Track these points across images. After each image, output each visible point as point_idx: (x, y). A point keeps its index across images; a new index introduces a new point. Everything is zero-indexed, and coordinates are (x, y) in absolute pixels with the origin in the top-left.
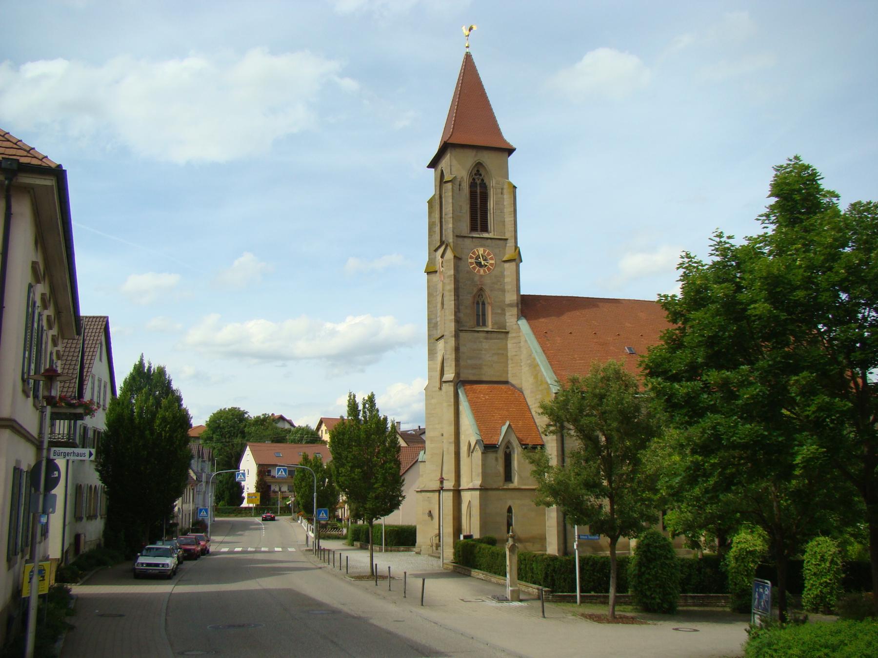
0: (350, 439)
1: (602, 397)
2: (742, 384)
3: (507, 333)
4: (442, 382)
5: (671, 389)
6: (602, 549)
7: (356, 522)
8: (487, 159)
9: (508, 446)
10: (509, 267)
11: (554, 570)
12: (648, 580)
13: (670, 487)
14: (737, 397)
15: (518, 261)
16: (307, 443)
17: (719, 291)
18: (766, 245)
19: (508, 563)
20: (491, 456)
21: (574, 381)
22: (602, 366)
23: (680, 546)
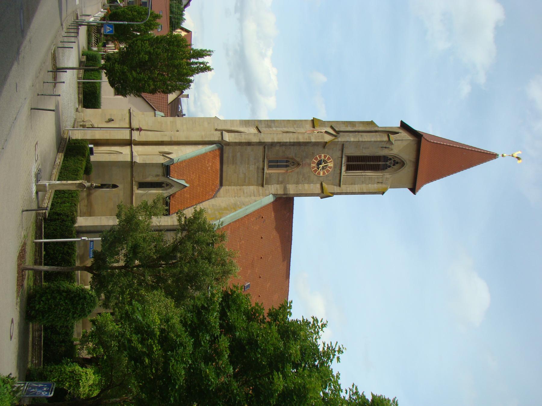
0: (173, 52)
1: (209, 259)
2: (219, 372)
3: (263, 186)
4: (222, 131)
5: (213, 309)
6: (82, 261)
7: (103, 58)
8: (407, 172)
9: (169, 185)
10: (317, 188)
11: (63, 220)
12: (54, 298)
13: (134, 312)
14: (206, 364)
15: (322, 195)
16: (170, 18)
17: (295, 349)
18: (332, 391)
19: (70, 182)
20: (160, 171)
21: (222, 237)
22: (235, 261)
23: (84, 327)
